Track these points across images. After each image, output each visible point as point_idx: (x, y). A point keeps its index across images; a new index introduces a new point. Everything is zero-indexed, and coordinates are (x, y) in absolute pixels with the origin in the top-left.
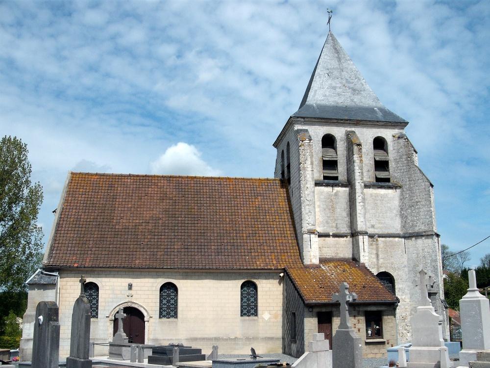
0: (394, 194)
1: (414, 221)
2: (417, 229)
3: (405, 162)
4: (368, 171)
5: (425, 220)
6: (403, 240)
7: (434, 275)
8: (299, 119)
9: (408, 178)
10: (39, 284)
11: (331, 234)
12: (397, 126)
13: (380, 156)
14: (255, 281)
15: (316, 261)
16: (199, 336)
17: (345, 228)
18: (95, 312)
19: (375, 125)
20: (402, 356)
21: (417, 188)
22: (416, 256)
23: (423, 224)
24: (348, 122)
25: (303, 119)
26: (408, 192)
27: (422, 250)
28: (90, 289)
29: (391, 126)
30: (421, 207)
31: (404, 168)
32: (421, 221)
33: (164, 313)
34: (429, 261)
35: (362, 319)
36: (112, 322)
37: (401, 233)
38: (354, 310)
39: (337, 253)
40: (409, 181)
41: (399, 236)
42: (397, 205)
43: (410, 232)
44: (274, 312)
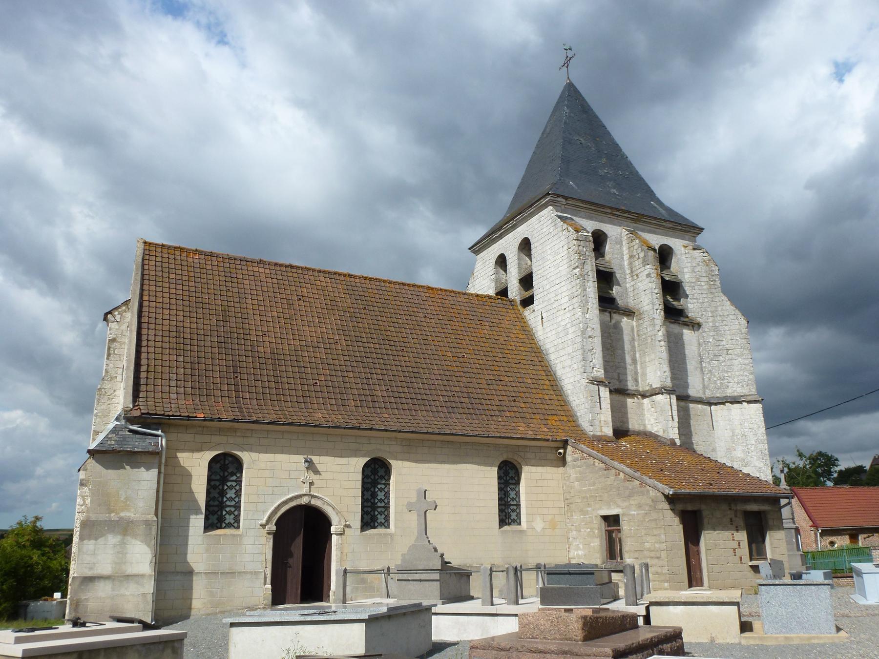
1: (724, 379)
2: (729, 392)
3: (705, 287)
5: (741, 378)
7: (762, 464)
8: (559, 199)
9: (712, 312)
10: (119, 452)
12: (689, 232)
14: (391, 461)
18: (232, 516)
19: (661, 226)
20: (337, 555)
21: (727, 328)
23: (739, 383)
27: (741, 424)
29: (681, 230)
31: (705, 296)
32: (736, 379)
34: (753, 442)
35: (847, 537)
36: (271, 537)
38: (730, 509)
44: (550, 517)
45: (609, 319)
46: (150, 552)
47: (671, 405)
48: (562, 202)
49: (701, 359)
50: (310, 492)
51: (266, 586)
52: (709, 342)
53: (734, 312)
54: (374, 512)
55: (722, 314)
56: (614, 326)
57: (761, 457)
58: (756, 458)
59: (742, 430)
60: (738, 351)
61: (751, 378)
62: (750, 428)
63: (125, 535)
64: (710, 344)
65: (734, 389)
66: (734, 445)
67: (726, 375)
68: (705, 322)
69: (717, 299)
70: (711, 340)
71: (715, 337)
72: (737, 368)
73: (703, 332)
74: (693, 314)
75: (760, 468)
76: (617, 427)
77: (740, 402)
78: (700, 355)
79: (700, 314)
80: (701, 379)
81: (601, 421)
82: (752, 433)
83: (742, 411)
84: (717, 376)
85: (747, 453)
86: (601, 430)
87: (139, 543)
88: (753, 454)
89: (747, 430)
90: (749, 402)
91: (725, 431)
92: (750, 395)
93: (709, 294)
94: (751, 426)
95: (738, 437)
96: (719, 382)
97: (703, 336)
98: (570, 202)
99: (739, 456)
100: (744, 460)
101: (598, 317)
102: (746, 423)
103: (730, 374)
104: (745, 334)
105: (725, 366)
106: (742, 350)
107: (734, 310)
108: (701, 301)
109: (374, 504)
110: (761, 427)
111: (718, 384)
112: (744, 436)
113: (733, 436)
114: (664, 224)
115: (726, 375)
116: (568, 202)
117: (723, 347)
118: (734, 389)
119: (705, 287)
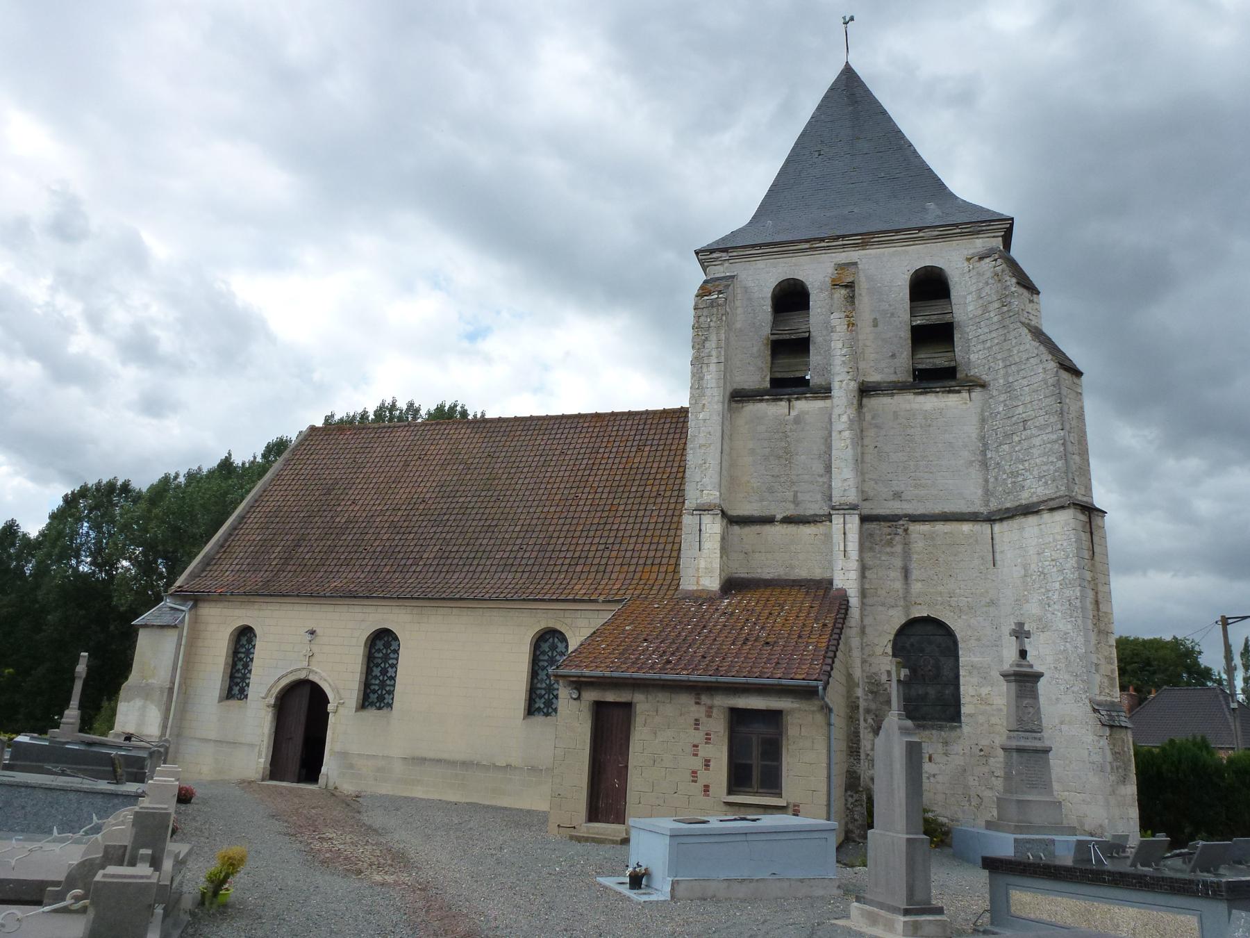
0: (964, 407)
1: (1018, 475)
2: (1025, 498)
4: (893, 356)
5: (1045, 468)
6: (986, 527)
8: (715, 255)
9: (1004, 360)
11: (779, 517)
12: (978, 232)
13: (930, 315)
15: (712, 583)
16: (431, 755)
17: (816, 502)
21: (1025, 382)
22: (1023, 572)
23: (1040, 478)
24: (841, 243)
25: (724, 254)
26: (1002, 399)
28: (244, 637)
29: (962, 234)
30: (1034, 431)
32: (1036, 473)
33: (373, 697)
34: (1057, 585)
36: (270, 709)
37: (984, 510)
38: (697, 703)
39: (792, 567)
40: (1005, 367)
41: (973, 518)
42: (974, 435)
43: (1008, 505)
45: (787, 411)
46: (159, 715)
47: (845, 534)
48: (721, 257)
49: (985, 445)
50: (308, 666)
51: (260, 760)
52: (998, 413)
53: (1036, 352)
54: (549, 695)
55: (1018, 360)
56: (794, 419)
57: (1069, 612)
58: (1059, 614)
59: (1040, 564)
60: (1041, 421)
61: (1061, 465)
62: (1052, 560)
63: (146, 700)
64: (999, 415)
65: (1034, 491)
66: (1026, 593)
67: (1021, 467)
68: (993, 380)
69: (1011, 336)
70: (1001, 409)
71: (1007, 402)
72: (1039, 451)
73: (990, 398)
74: (976, 370)
75: (1066, 634)
76: (779, 575)
77: (1037, 512)
78: (982, 438)
79: (987, 367)
80: (981, 481)
81: (698, 569)
82: (1055, 569)
83: (1041, 530)
84: (1008, 471)
85: (1047, 606)
86: (697, 582)
87: (154, 707)
88: (1056, 607)
89: (1047, 563)
90: (1052, 510)
91: (1014, 567)
92: (1057, 498)
93: (1000, 330)
94: (1055, 555)
95: (1034, 577)
96: (1009, 481)
97: (990, 405)
98: (735, 254)
99: (1033, 612)
100: (1040, 620)
101: (719, 415)
102: (1046, 550)
103: (1026, 464)
104: (1052, 388)
105: (1019, 451)
106: (1047, 416)
107: (1037, 348)
108: (988, 344)
109: (383, 681)
110: (1071, 556)
111: (1009, 486)
112: (1042, 575)
113: (1025, 576)
114: (921, 234)
115: (1021, 467)
116: (731, 254)
117: (1018, 418)
118: (1032, 490)
119: (995, 319)
